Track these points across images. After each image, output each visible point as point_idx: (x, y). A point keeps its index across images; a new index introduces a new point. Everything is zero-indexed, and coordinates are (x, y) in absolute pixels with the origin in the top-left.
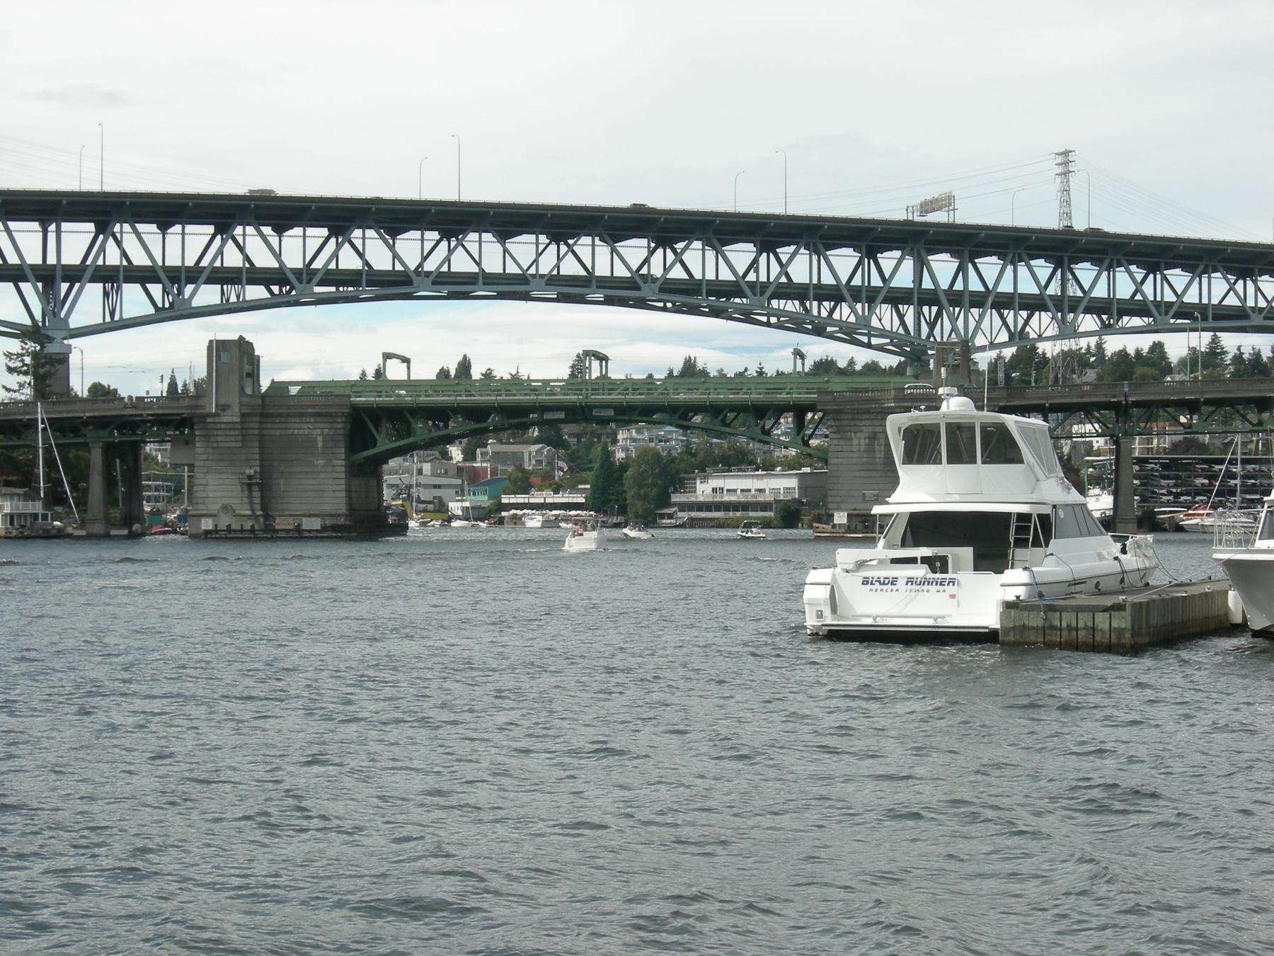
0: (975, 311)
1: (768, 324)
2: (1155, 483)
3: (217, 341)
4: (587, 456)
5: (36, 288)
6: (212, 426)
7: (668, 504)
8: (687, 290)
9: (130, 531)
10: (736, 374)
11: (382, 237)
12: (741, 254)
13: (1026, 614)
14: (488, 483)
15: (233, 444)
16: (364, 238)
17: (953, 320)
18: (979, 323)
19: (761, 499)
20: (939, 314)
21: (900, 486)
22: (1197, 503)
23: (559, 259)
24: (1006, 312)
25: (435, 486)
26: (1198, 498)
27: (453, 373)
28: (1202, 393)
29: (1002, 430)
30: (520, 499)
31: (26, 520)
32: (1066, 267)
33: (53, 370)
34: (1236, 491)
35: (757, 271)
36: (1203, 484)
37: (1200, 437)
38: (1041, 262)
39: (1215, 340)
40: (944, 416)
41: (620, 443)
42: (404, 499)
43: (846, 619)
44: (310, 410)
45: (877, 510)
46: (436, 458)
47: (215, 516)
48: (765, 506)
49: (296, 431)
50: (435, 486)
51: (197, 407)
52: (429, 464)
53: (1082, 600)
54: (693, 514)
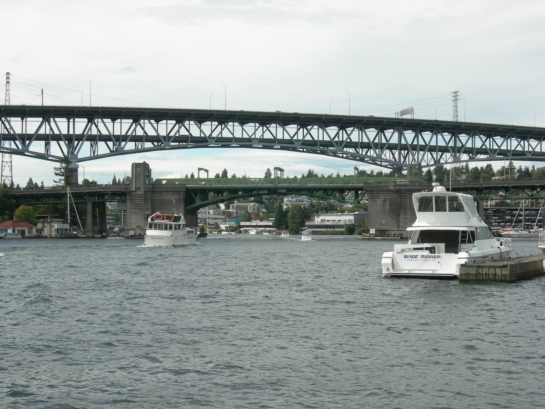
0: (421, 152)
1: (343, 157)
2: (491, 218)
3: (135, 163)
4: (272, 207)
5: (65, 143)
6: (133, 195)
7: (305, 226)
8: (312, 144)
9: (102, 235)
10: (328, 176)
11: (196, 124)
12: (332, 130)
13: (469, 269)
14: (235, 217)
15: (141, 203)
16: (189, 124)
17: (413, 156)
18: (423, 157)
19: (339, 224)
20: (408, 154)
21: (417, 220)
22: (507, 226)
23: (263, 133)
24: (433, 153)
25: (215, 219)
26: (507, 224)
27: (221, 176)
28: (510, 184)
29: (456, 198)
30: (248, 223)
31: (63, 231)
32: (456, 136)
33: (72, 174)
34: (522, 221)
35: (338, 137)
36: (509, 219)
37: (506, 200)
38: (446, 134)
39: (511, 164)
40: (435, 193)
41: (285, 202)
42: (203, 224)
43: (399, 271)
44: (170, 190)
45: (409, 229)
46: (215, 208)
47: (135, 230)
48: (341, 226)
50: (215, 219)
51: (128, 188)
52: (212, 210)
53: (489, 263)
54: (314, 229)
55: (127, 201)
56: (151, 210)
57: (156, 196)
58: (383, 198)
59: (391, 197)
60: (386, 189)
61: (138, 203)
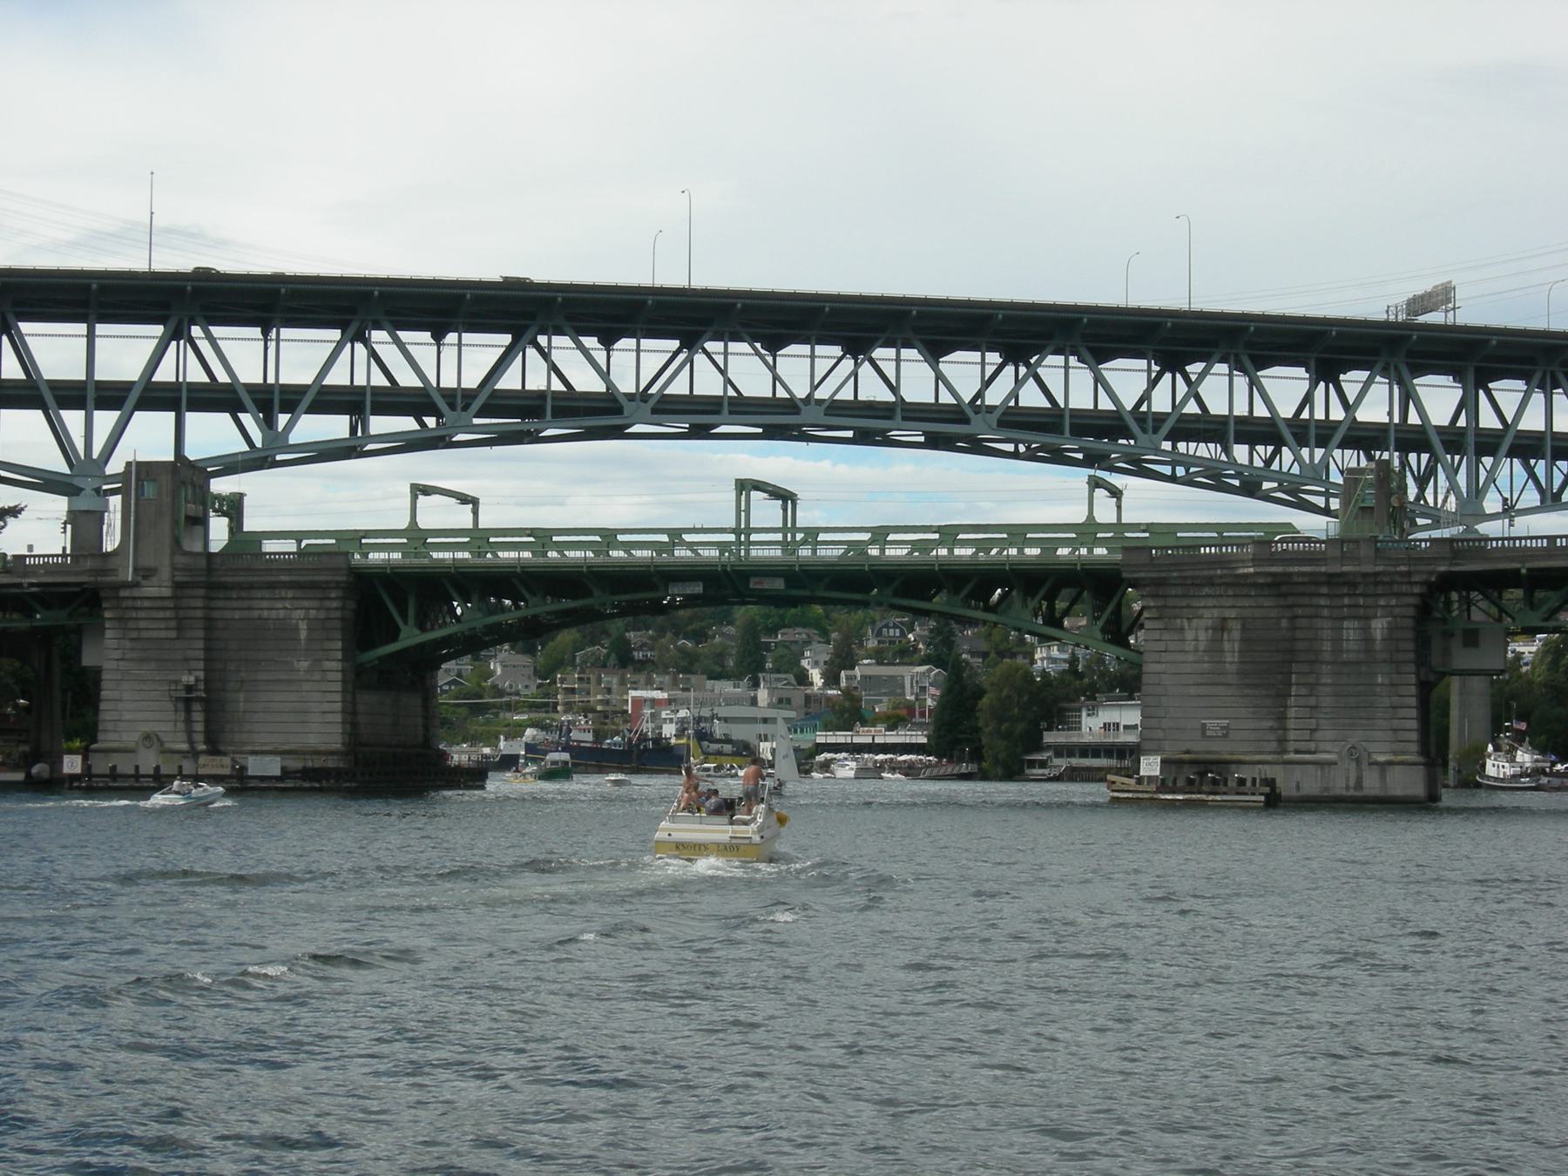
0: (1488, 461)
1: (1173, 479)
3: (139, 464)
6: (129, 603)
7: (1038, 746)
8: (1046, 424)
9: (28, 775)
11: (757, 353)
15: (163, 634)
24: (1532, 462)
30: (841, 737)
44: (284, 578)
49: (265, 613)
54: (1076, 762)
55: (107, 625)
56: (201, 665)
57: (229, 604)
58: (1210, 615)
59: (1247, 613)
60: (1221, 576)
61: (145, 634)
